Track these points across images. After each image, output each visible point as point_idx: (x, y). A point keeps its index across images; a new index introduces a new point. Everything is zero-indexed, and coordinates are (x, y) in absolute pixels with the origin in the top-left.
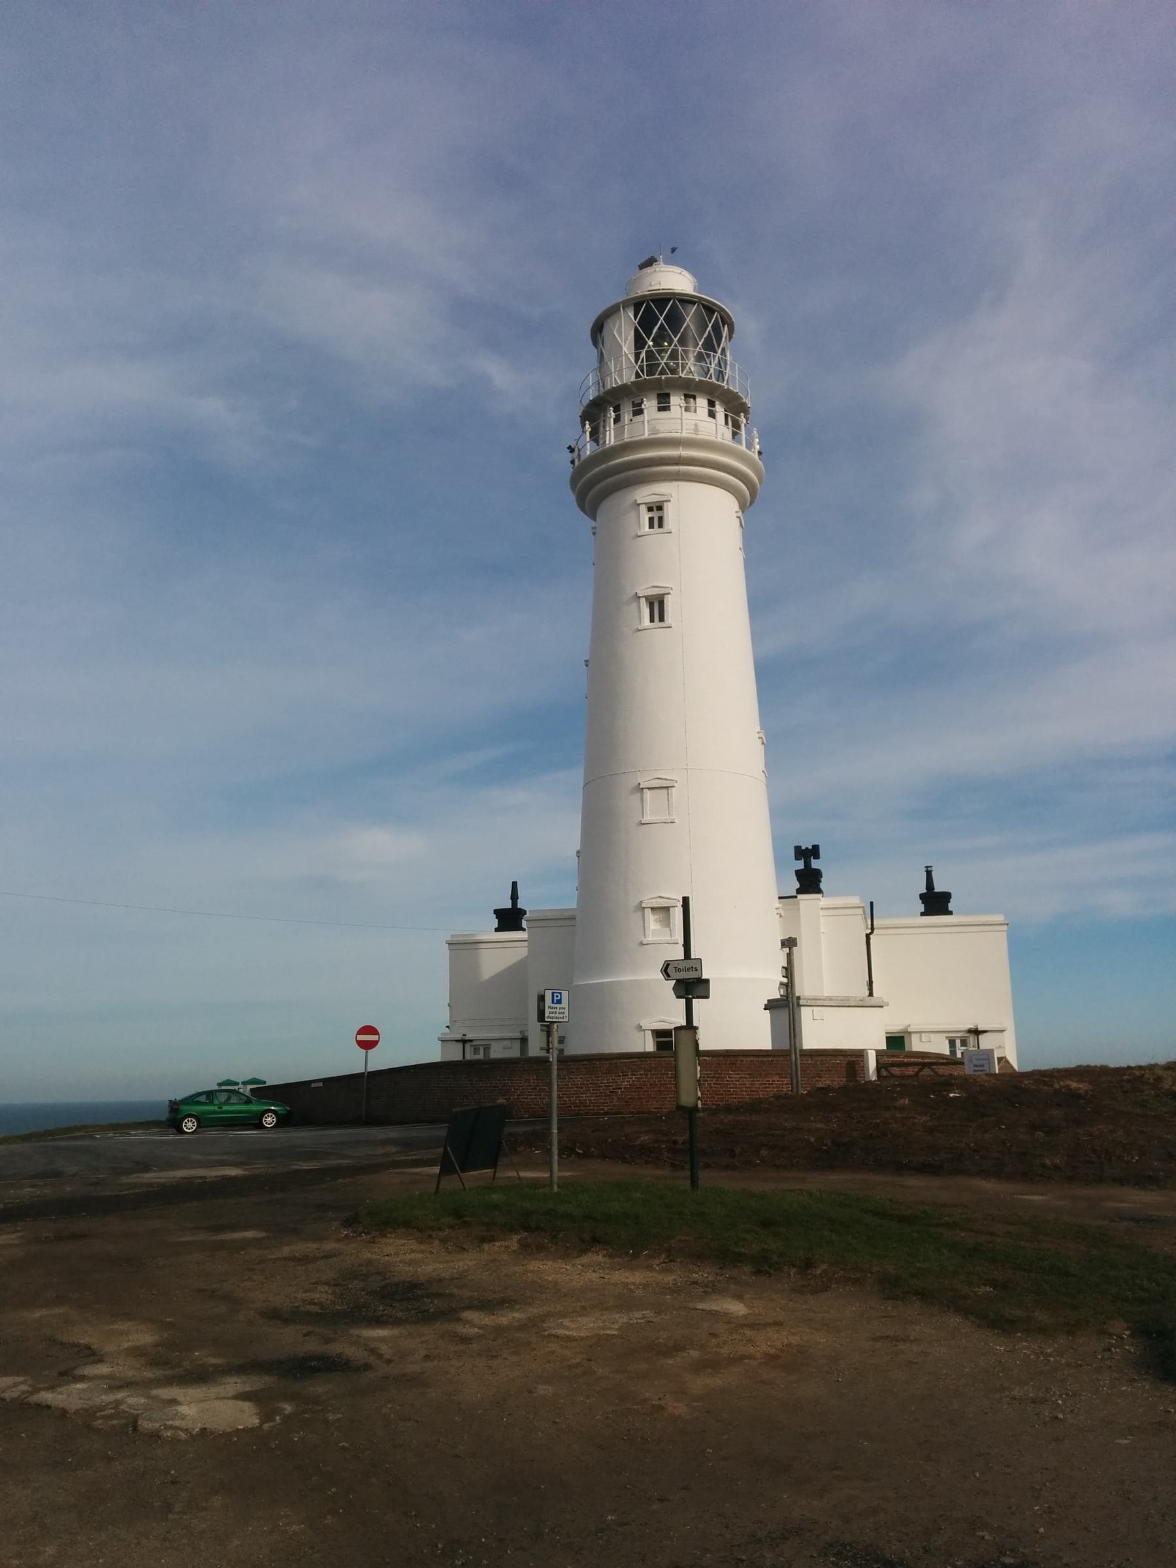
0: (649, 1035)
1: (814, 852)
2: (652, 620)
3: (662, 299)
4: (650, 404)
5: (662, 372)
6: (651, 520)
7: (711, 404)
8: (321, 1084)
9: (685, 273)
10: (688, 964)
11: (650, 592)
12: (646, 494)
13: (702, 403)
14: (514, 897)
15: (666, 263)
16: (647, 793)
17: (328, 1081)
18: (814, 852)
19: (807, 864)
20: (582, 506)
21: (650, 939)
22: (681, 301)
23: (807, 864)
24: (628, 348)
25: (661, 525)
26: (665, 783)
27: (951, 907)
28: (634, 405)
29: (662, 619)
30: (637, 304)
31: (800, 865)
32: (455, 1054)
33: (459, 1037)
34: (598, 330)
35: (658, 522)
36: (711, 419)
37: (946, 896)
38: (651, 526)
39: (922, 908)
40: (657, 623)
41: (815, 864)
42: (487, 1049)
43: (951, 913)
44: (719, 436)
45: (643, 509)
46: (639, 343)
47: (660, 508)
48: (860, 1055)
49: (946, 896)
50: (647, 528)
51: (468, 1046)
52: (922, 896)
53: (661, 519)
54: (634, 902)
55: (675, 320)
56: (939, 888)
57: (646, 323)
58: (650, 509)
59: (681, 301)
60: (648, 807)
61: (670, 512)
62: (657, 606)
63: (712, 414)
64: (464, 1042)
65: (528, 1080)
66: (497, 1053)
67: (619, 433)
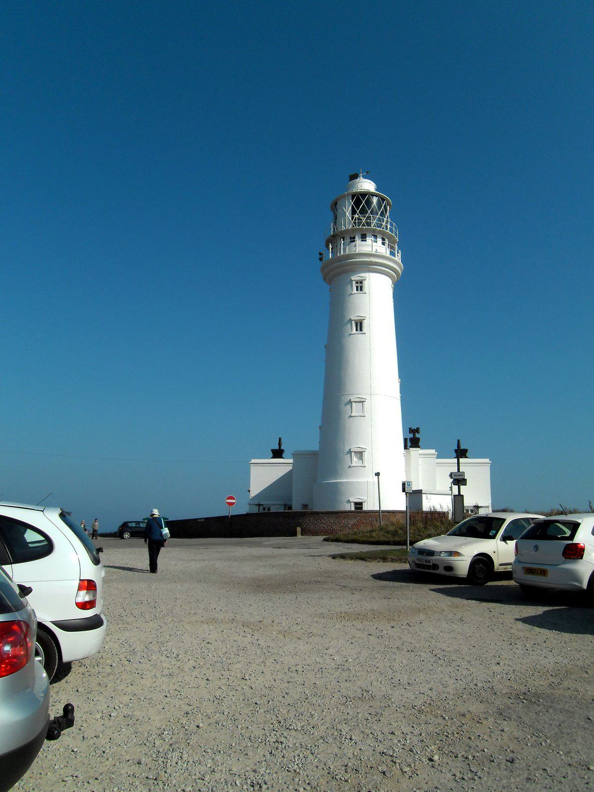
0: (353, 504)
1: (417, 431)
2: (357, 330)
3: (364, 195)
4: (358, 241)
5: (364, 225)
6: (357, 287)
7: (383, 239)
8: (203, 520)
9: (372, 183)
10: (459, 473)
11: (356, 318)
12: (355, 278)
13: (379, 240)
14: (280, 444)
15: (364, 177)
16: (354, 404)
17: (206, 519)
18: (417, 431)
19: (414, 435)
20: (325, 279)
21: (354, 464)
22: (371, 195)
23: (414, 435)
24: (348, 214)
25: (361, 290)
26: (362, 400)
27: (467, 455)
28: (351, 238)
29: (361, 330)
30: (353, 196)
31: (411, 436)
32: (255, 510)
33: (257, 503)
34: (335, 205)
35: (360, 288)
36: (383, 246)
37: (376, 475)
38: (357, 290)
39: (271, 455)
40: (359, 332)
41: (417, 435)
42: (269, 509)
43: (466, 457)
44: (374, 250)
45: (354, 283)
46: (354, 212)
47: (361, 282)
48: (302, 534)
49: (376, 475)
50: (355, 291)
51: (261, 507)
52: (456, 451)
53: (361, 287)
54: (347, 449)
55: (369, 203)
56: (462, 447)
57: (357, 203)
58: (357, 283)
59: (371, 195)
60: (354, 410)
61: (366, 284)
62: (359, 325)
63: (383, 244)
64: (259, 505)
65: (310, 520)
66: (273, 510)
67: (345, 250)
